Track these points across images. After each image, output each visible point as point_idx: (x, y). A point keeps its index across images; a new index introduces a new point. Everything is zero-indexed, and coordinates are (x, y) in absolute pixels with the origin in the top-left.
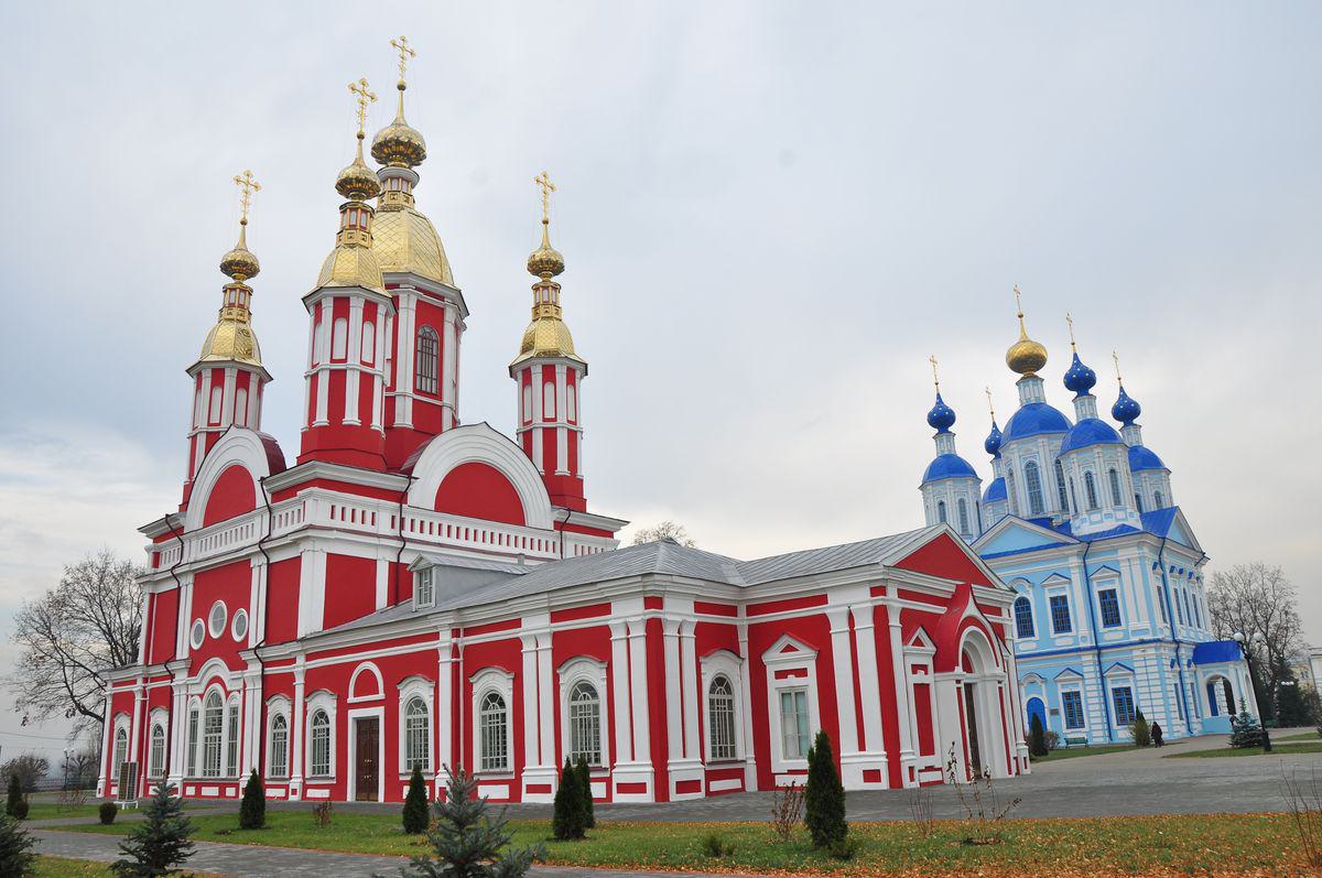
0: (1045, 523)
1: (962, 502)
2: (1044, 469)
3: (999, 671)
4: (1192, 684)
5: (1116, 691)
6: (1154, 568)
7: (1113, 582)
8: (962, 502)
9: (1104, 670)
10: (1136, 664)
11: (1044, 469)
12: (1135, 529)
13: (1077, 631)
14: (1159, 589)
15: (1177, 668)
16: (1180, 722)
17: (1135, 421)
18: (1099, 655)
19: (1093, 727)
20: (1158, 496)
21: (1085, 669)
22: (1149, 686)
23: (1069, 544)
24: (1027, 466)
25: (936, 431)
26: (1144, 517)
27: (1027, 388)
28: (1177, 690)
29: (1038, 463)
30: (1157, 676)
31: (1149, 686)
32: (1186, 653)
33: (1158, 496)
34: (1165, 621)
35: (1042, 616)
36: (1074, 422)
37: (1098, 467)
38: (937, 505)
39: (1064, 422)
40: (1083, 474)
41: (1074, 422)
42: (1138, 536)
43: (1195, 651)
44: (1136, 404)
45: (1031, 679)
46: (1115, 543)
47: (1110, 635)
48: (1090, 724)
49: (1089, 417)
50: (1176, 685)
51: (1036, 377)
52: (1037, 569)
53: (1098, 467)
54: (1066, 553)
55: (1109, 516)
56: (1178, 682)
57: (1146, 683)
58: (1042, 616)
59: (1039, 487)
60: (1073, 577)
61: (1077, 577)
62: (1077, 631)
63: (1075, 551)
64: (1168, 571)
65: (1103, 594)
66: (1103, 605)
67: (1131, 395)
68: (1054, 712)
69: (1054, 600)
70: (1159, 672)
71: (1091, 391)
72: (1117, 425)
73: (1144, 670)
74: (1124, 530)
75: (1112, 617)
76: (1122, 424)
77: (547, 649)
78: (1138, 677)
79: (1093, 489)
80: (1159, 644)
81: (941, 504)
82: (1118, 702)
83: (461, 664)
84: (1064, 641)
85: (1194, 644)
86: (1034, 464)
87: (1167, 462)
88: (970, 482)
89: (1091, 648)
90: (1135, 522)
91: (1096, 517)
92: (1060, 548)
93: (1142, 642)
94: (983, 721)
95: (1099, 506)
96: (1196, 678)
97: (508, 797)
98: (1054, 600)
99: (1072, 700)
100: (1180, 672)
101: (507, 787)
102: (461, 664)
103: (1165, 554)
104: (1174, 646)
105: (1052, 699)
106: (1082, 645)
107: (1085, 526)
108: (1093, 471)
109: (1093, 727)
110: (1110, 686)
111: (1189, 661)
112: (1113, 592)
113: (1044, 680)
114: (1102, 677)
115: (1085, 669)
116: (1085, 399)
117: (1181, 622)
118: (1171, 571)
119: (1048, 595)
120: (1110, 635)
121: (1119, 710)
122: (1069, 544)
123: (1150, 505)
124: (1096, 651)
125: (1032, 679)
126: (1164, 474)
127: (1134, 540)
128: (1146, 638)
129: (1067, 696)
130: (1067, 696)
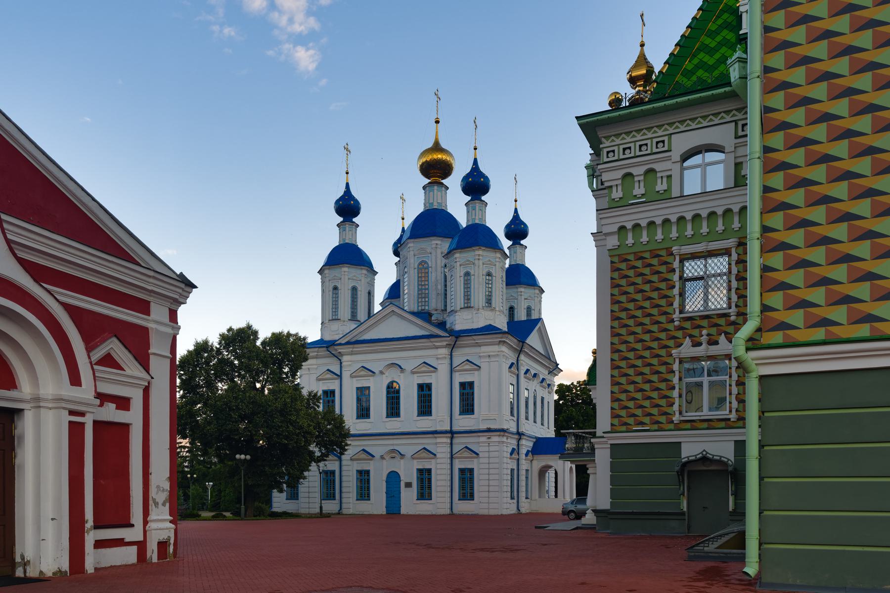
0: (424, 315)
1: (354, 289)
4: (527, 470)
5: (462, 471)
6: (510, 367)
8: (354, 289)
9: (454, 452)
12: (499, 329)
15: (515, 456)
16: (511, 501)
17: (522, 242)
18: (452, 438)
20: (529, 310)
21: (439, 450)
23: (440, 336)
24: (420, 264)
25: (341, 219)
26: (511, 322)
28: (512, 476)
32: (527, 445)
33: (529, 310)
34: (512, 414)
35: (409, 401)
36: (464, 225)
38: (331, 289)
41: (464, 225)
42: (500, 335)
43: (535, 444)
44: (486, 178)
45: (393, 455)
46: (480, 339)
47: (463, 422)
49: (477, 221)
50: (512, 470)
51: (442, 184)
52: (411, 358)
54: (437, 344)
56: (515, 467)
58: (409, 401)
61: (443, 368)
63: (445, 343)
66: (462, 395)
68: (408, 485)
72: (506, 243)
73: (486, 455)
74: (489, 330)
75: (468, 407)
76: (510, 243)
80: (502, 433)
81: (335, 288)
82: (462, 480)
83: (90, 524)
84: (425, 424)
85: (536, 438)
86: (426, 262)
87: (542, 282)
88: (364, 272)
89: (445, 432)
90: (502, 323)
92: (432, 340)
93: (489, 430)
94: (120, 346)
96: (532, 467)
99: (425, 476)
100: (518, 459)
102: (90, 524)
103: (522, 357)
104: (517, 437)
105: (408, 472)
106: (439, 428)
107: (461, 321)
111: (528, 451)
113: (402, 456)
114: (452, 458)
116: (477, 204)
117: (527, 418)
118: (526, 373)
120: (463, 422)
121: (462, 487)
122: (440, 336)
123: (521, 316)
124: (450, 435)
125: (396, 454)
126: (537, 291)
127: (497, 338)
128: (493, 427)
129: (420, 471)
130: (420, 471)
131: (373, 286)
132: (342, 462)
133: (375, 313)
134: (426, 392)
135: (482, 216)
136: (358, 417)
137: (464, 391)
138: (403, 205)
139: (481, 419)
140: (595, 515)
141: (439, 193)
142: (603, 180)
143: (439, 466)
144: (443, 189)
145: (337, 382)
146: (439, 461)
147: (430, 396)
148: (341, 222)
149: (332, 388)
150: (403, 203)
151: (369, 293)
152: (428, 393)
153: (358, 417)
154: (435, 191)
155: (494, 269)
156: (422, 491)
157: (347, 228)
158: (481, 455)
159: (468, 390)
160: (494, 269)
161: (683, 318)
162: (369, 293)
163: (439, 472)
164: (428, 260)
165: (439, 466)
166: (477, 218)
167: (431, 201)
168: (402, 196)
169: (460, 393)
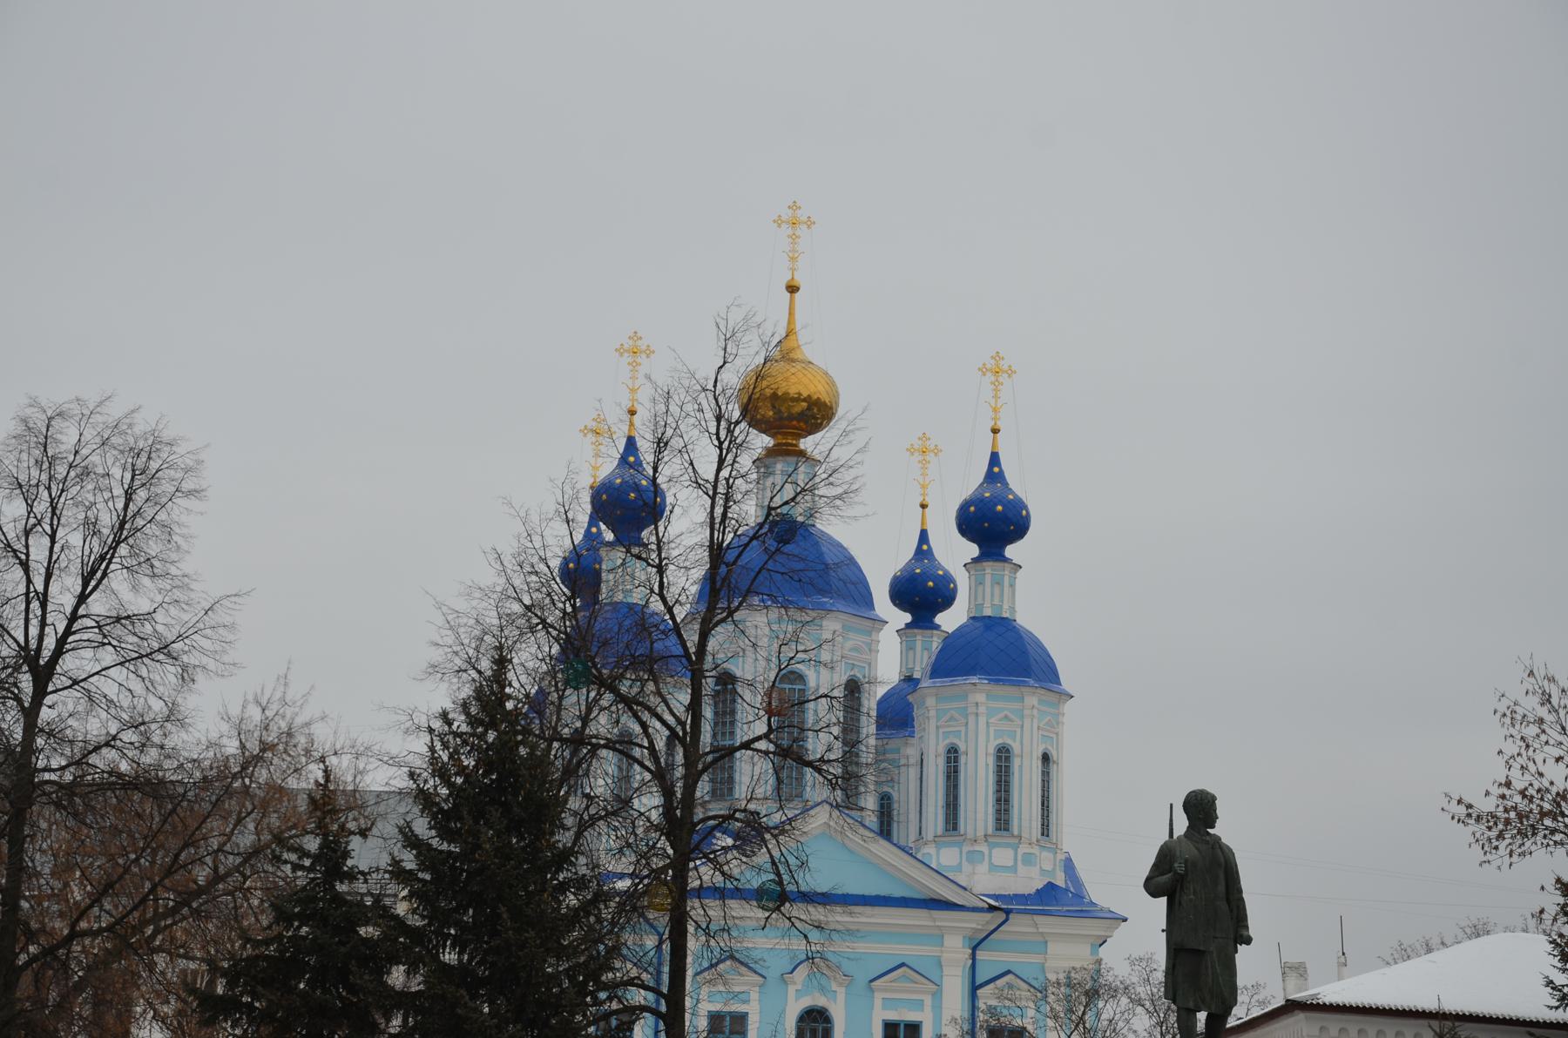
1: (1003, 756)
40: (942, 749)
51: (802, 454)
55: (1029, 860)
67: (1019, 483)
71: (1011, 551)
79: (999, 782)
116: (990, 567)
148: (975, 560)
151: (1046, 758)
157: (988, 579)
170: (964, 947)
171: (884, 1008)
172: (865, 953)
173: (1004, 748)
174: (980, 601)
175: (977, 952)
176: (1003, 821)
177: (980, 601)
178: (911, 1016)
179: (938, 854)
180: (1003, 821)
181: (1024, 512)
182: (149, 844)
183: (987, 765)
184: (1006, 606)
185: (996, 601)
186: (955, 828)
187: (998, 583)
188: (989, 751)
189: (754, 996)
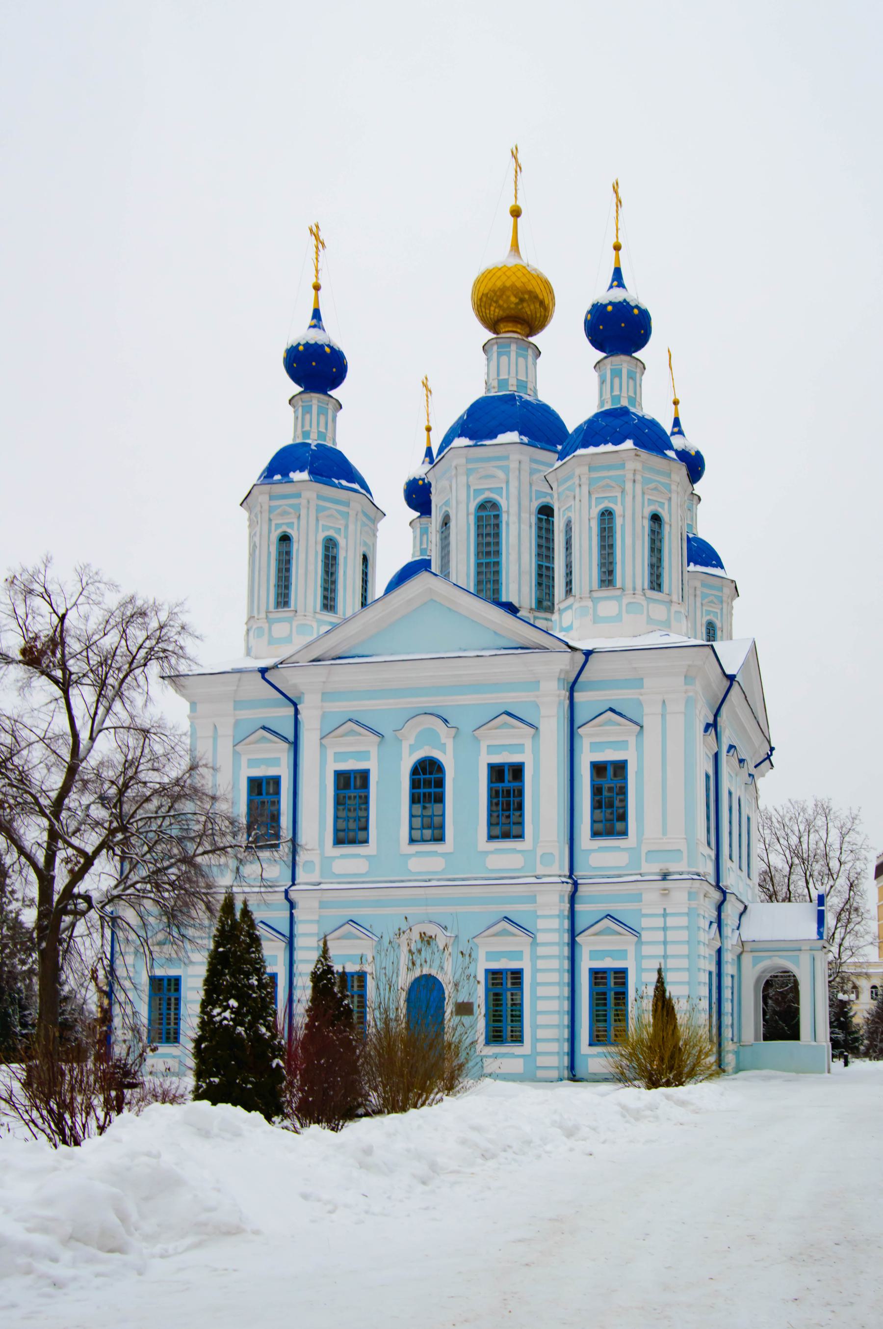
1: (330, 545)
2: (513, 519)
3: (7, 780)
7: (623, 745)
8: (330, 545)
10: (645, 922)
11: (513, 519)
13: (640, 841)
14: (707, 777)
19: (541, 1047)
22: (665, 929)
23: (620, 934)
24: (482, 507)
27: (504, 359)
29: (504, 507)
30: (684, 963)
31: (665, 929)
37: (629, 499)
39: (352, 472)
48: (535, 1040)
50: (710, 973)
53: (629, 499)
57: (660, 922)
59: (498, 553)
60: (543, 727)
62: (640, 841)
64: (725, 748)
65: (598, 769)
66: (597, 791)
69: (497, 772)
70: (688, 956)
77: (198, 976)
78: (646, 950)
82: (598, 999)
86: (495, 505)
91: (608, 607)
95: (618, 584)
97: (589, 1059)
98: (497, 772)
101: (521, 1060)
108: (617, 509)
109: (541, 1047)
110: (585, 965)
112: (620, 767)
114: (573, 934)
115: (541, 924)
119: (486, 759)
121: (598, 1017)
131: (374, 545)
132: (295, 966)
133: (376, 598)
134: (508, 783)
135: (635, 393)
136: (339, 841)
137: (500, 786)
138: (427, 401)
139: (644, 851)
140: (870, 1060)
141: (521, 361)
142: (116, 882)
143: (541, 964)
144: (530, 352)
145: (283, 752)
146: (541, 951)
147: (520, 793)
148: (300, 393)
149: (271, 772)
150: (427, 396)
151: (365, 559)
152: (516, 784)
153: (339, 841)
154: (513, 355)
155: (666, 506)
156: (497, 1024)
158: (646, 936)
159: (508, 783)
160: (666, 506)
161: (349, 778)
162: (365, 559)
163: (541, 978)
164: (501, 495)
165: (541, 964)
166: (624, 394)
167: (503, 376)
168: (425, 382)
169: (490, 789)
170: (559, 689)
171: (489, 753)
172: (436, 706)
173: (606, 511)
174: (616, 392)
175: (576, 695)
176: (607, 576)
177: (616, 392)
178: (515, 758)
179: (270, 629)
180: (607, 576)
181: (636, 311)
182: (111, 666)
183: (590, 528)
184: (329, 435)
185: (631, 394)
186: (286, 604)
187: (631, 378)
188: (592, 516)
189: (374, 751)
